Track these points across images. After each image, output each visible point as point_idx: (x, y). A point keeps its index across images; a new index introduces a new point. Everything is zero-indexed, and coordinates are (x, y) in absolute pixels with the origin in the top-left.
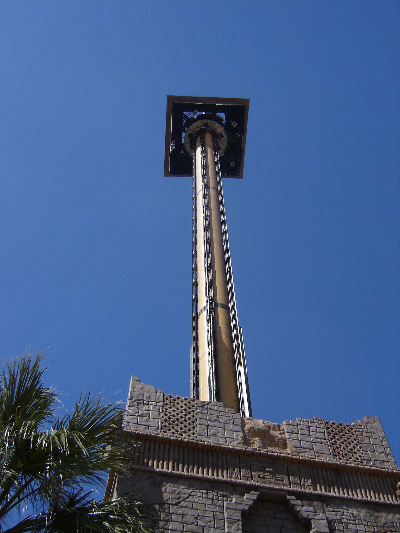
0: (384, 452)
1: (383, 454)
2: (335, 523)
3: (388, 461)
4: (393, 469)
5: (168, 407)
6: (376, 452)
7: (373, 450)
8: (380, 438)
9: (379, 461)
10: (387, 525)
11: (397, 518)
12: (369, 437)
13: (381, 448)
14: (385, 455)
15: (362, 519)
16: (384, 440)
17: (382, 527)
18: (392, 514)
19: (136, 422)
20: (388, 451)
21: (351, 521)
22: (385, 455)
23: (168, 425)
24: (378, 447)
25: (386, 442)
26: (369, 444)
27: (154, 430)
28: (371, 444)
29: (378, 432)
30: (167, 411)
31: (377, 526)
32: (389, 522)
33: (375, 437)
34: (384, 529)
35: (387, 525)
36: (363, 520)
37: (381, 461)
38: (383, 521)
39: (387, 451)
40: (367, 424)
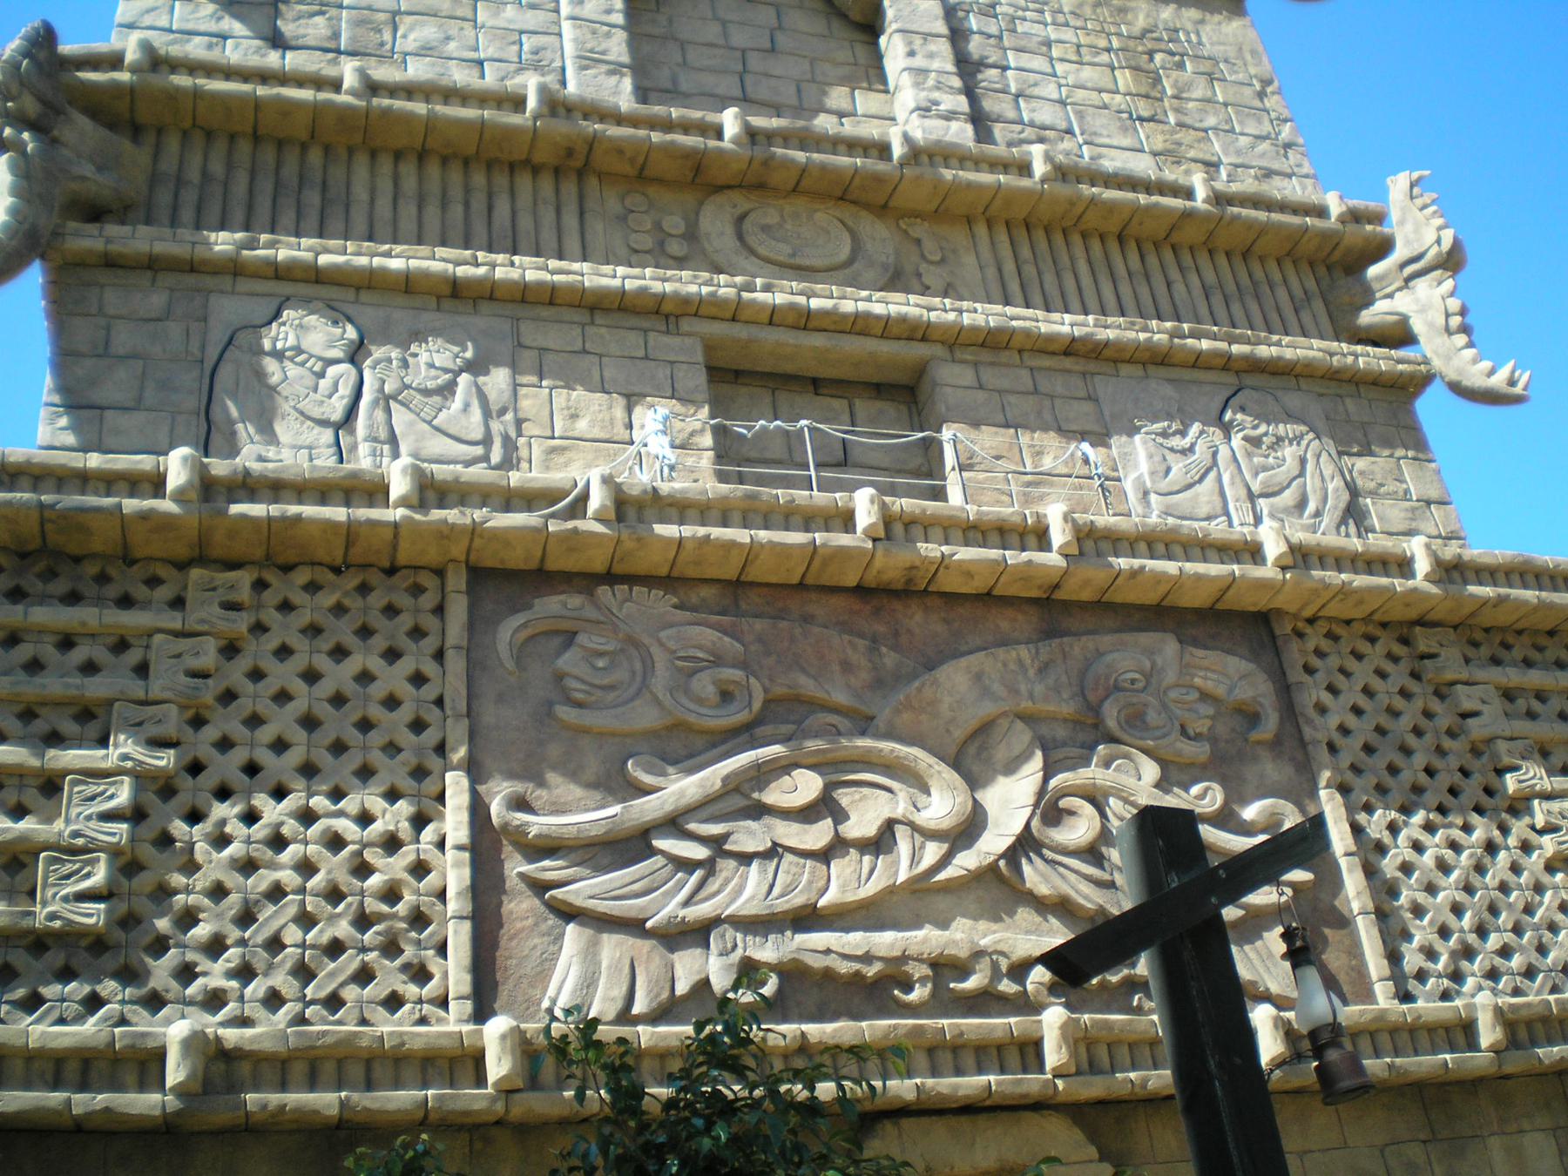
0: (1273, 136)
1: (1264, 146)
2: (968, 12)
3: (1289, 171)
4: (1374, 357)
5: (341, 979)
6: (1242, 134)
7: (1227, 127)
8: (1255, 81)
9: (1252, 171)
10: (1154, 35)
11: (1189, 19)
12: (1209, 75)
13: (1259, 121)
14: (1276, 146)
15: (1066, 9)
16: (1269, 90)
17: (1136, 38)
18: (1172, 7)
19: (164, 22)
20: (1286, 132)
21: (1028, 13)
22: (1274, 148)
23: (352, 931)
24: (1248, 115)
25: (1276, 97)
26: (1208, 101)
27: (251, 51)
28: (1218, 102)
29: (1243, 59)
30: (342, 804)
31: (1119, 35)
32: (1161, 26)
33: (1233, 78)
34: (1144, 45)
35: (1154, 35)
36: (1072, 13)
37: (1260, 168)
38: (1141, 22)
39: (1283, 135)
40: (1199, 27)
